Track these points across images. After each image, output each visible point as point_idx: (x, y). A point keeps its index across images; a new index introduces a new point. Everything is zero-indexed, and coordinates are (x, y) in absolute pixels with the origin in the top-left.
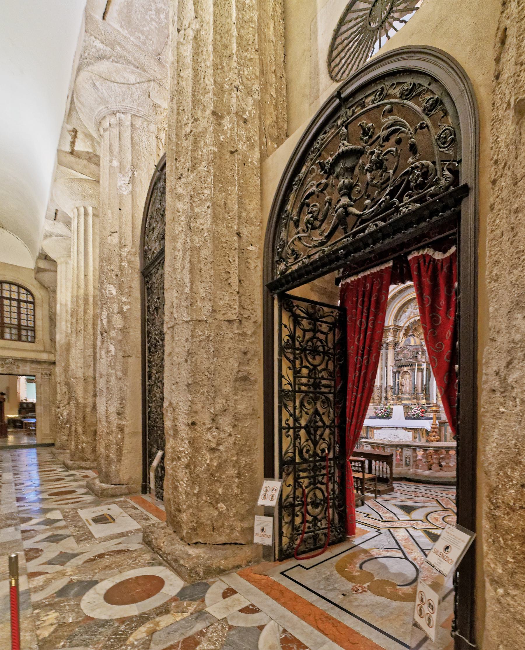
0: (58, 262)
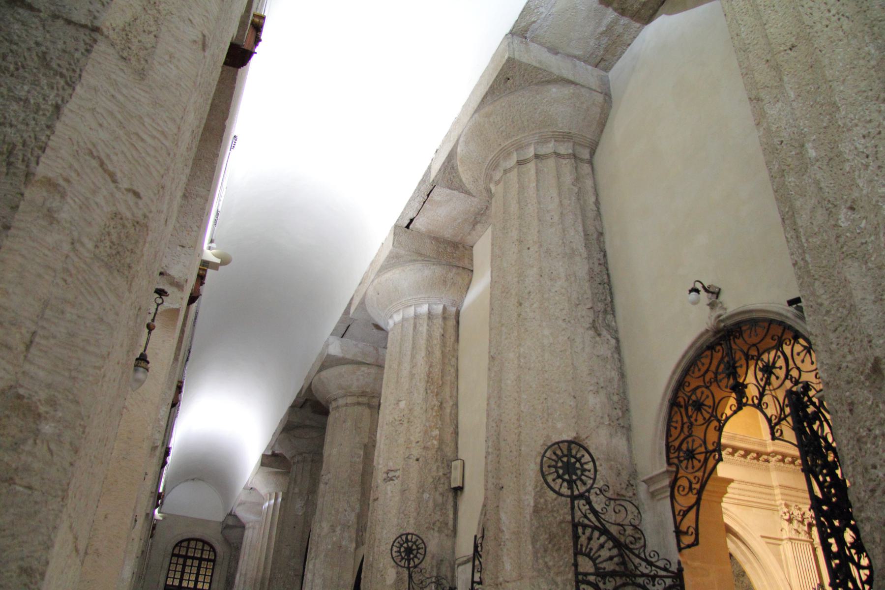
0: (247, 526)
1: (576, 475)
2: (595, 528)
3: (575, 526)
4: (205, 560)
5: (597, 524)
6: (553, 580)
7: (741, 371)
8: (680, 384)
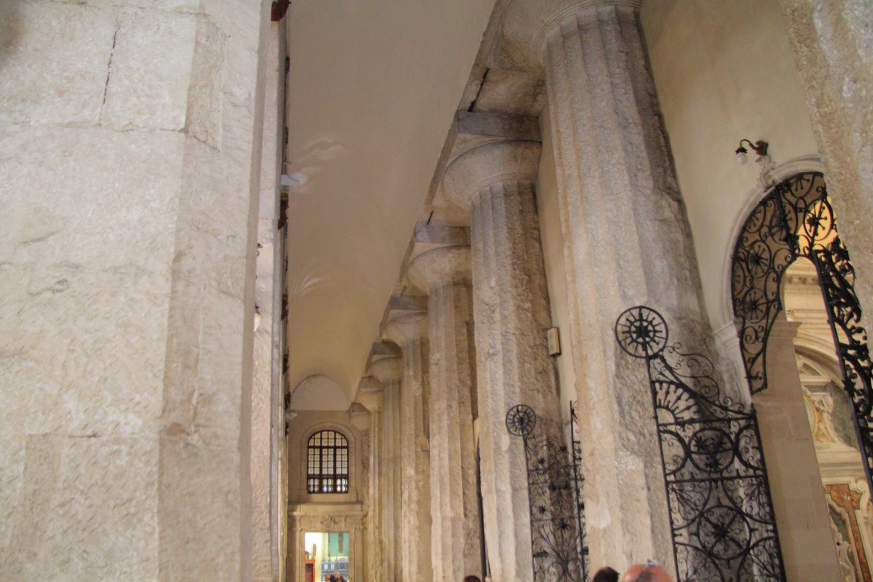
1: (649, 337)
2: (671, 383)
3: (653, 383)
4: (339, 447)
5: (672, 378)
6: (640, 432)
7: (792, 225)
8: (740, 240)
